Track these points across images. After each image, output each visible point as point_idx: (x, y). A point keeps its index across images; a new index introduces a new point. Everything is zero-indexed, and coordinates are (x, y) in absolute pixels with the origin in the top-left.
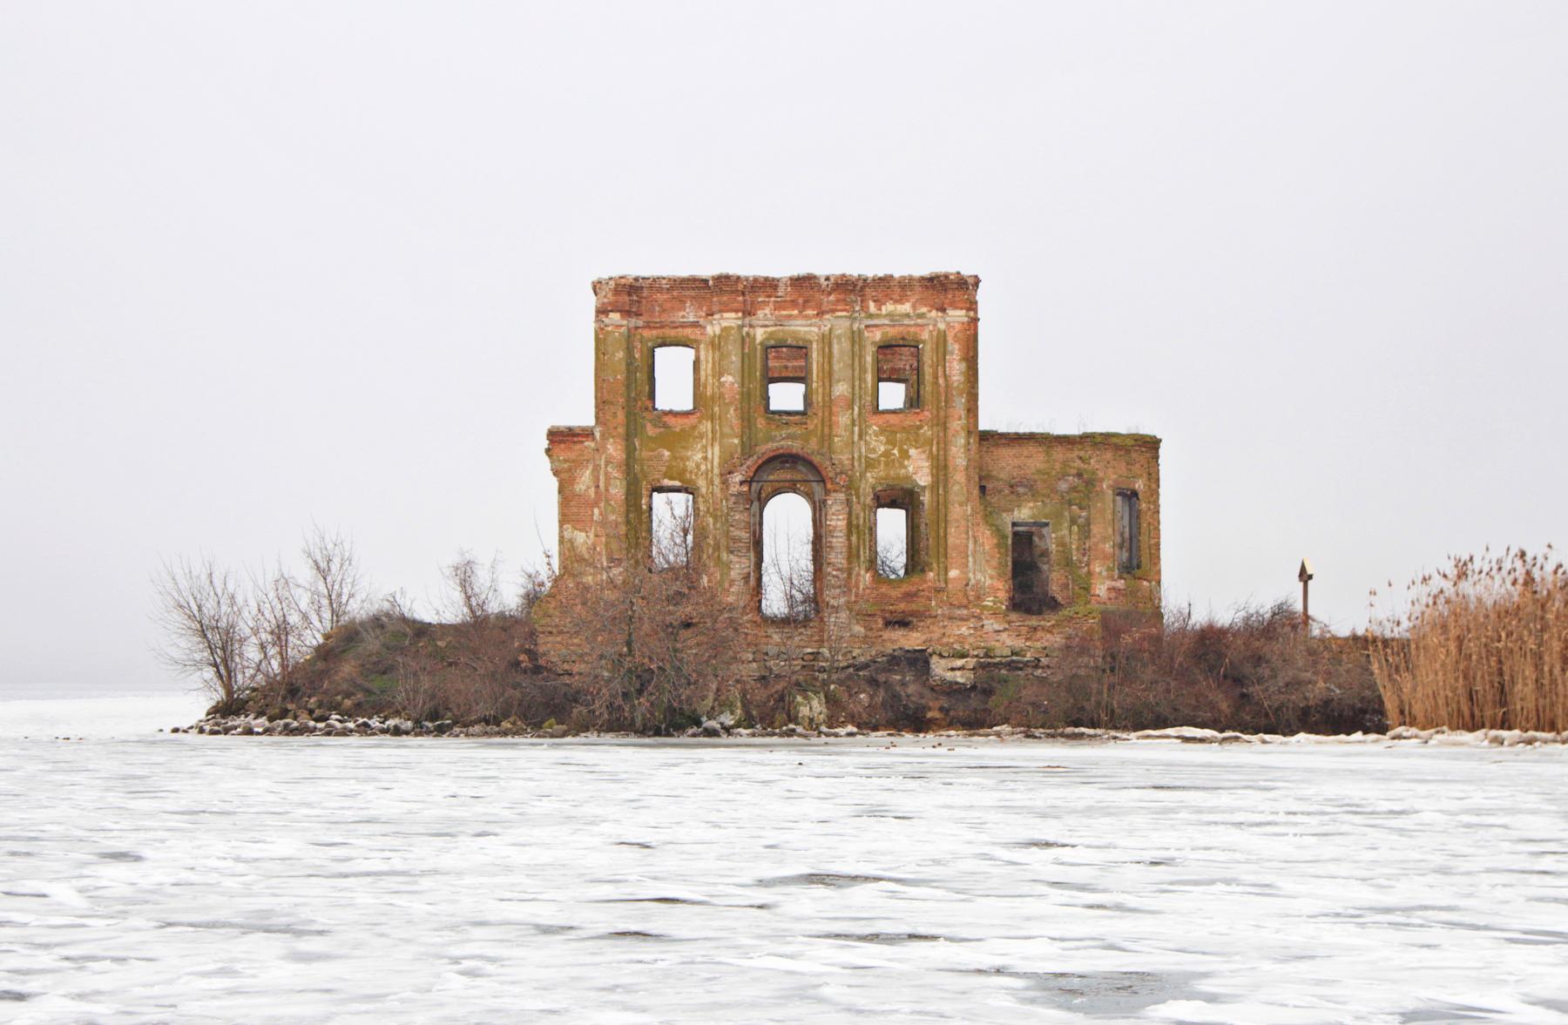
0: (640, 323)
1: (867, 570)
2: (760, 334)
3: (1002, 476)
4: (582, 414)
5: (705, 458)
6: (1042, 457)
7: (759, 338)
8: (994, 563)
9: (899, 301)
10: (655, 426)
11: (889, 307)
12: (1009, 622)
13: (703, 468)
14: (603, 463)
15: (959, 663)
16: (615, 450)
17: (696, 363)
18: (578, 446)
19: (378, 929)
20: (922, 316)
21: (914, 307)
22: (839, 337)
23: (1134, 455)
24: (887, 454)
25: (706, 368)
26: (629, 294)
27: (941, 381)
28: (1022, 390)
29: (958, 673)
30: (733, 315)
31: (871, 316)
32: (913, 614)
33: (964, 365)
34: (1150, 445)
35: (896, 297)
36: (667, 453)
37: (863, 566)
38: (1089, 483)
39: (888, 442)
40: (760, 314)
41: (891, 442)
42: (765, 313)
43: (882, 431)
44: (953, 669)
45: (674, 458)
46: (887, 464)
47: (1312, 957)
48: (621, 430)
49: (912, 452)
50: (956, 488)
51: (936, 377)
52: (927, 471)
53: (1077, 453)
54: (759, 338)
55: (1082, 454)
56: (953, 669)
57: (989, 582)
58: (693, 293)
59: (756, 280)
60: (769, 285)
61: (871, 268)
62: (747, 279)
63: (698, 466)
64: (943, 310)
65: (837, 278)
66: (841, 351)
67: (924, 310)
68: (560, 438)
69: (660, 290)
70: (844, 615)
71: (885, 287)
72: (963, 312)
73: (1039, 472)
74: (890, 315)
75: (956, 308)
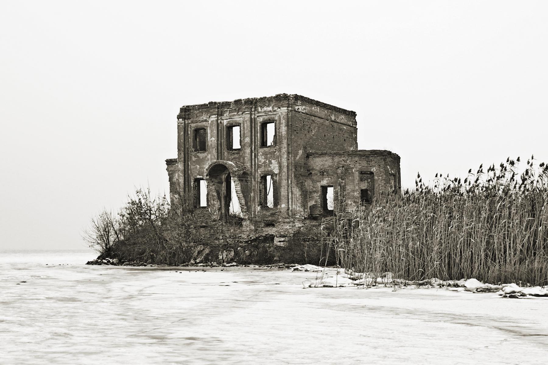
0: (190, 122)
1: (258, 206)
2: (225, 122)
3: (318, 168)
4: (174, 155)
6: (331, 161)
7: (225, 124)
8: (300, 201)
9: (268, 106)
10: (195, 157)
11: (265, 109)
12: (304, 224)
15: (282, 239)
18: (174, 166)
19: (357, 282)
20: (275, 111)
21: (273, 108)
22: (246, 121)
23: (371, 158)
24: (265, 162)
28: (366, 141)
29: (282, 243)
30: (214, 116)
31: (259, 113)
32: (273, 221)
33: (286, 128)
35: (267, 105)
36: (198, 166)
38: (347, 170)
40: (225, 115)
41: (266, 158)
42: (226, 115)
43: (263, 154)
44: (280, 242)
45: (200, 168)
46: (264, 166)
49: (273, 161)
50: (284, 174)
52: (277, 168)
53: (342, 158)
54: (225, 124)
55: (344, 158)
56: (280, 242)
57: (298, 208)
58: (205, 110)
59: (223, 103)
60: (227, 104)
61: (258, 95)
62: (219, 103)
64: (280, 108)
65: (246, 99)
66: (247, 126)
67: (276, 109)
68: (170, 162)
69: (196, 110)
70: (248, 222)
71: (264, 101)
72: (286, 108)
73: (329, 166)
74: (265, 112)
75: (283, 107)
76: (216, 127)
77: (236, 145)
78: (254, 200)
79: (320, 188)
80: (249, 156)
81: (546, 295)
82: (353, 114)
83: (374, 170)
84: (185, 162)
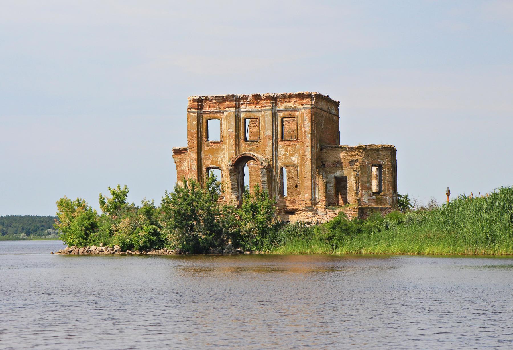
1: (279, 194)
3: (331, 161)
4: (183, 144)
5: (224, 157)
13: (223, 160)
14: (190, 160)
16: (194, 155)
17: (221, 124)
25: (224, 127)
26: (198, 102)
27: (303, 130)
30: (232, 109)
34: (392, 151)
37: (277, 193)
39: (285, 151)
41: (287, 150)
46: (285, 158)
47: (283, 271)
48: (196, 148)
51: (301, 128)
60: (245, 98)
63: (222, 160)
66: (268, 120)
68: (177, 152)
76: (234, 119)
77: (374, 169)
78: (275, 189)
79: (333, 179)
80: (270, 148)
81: (511, 267)
82: (336, 104)
83: (383, 162)
84: (198, 152)
